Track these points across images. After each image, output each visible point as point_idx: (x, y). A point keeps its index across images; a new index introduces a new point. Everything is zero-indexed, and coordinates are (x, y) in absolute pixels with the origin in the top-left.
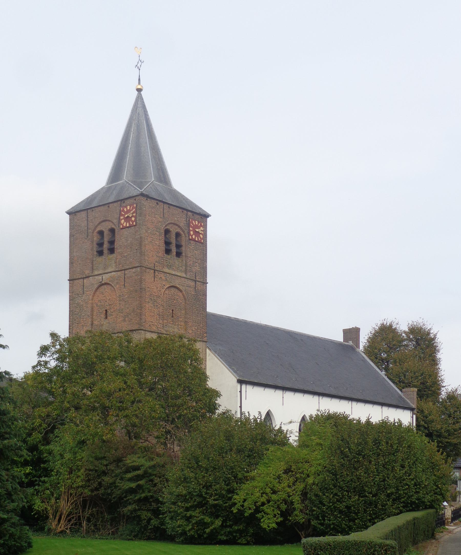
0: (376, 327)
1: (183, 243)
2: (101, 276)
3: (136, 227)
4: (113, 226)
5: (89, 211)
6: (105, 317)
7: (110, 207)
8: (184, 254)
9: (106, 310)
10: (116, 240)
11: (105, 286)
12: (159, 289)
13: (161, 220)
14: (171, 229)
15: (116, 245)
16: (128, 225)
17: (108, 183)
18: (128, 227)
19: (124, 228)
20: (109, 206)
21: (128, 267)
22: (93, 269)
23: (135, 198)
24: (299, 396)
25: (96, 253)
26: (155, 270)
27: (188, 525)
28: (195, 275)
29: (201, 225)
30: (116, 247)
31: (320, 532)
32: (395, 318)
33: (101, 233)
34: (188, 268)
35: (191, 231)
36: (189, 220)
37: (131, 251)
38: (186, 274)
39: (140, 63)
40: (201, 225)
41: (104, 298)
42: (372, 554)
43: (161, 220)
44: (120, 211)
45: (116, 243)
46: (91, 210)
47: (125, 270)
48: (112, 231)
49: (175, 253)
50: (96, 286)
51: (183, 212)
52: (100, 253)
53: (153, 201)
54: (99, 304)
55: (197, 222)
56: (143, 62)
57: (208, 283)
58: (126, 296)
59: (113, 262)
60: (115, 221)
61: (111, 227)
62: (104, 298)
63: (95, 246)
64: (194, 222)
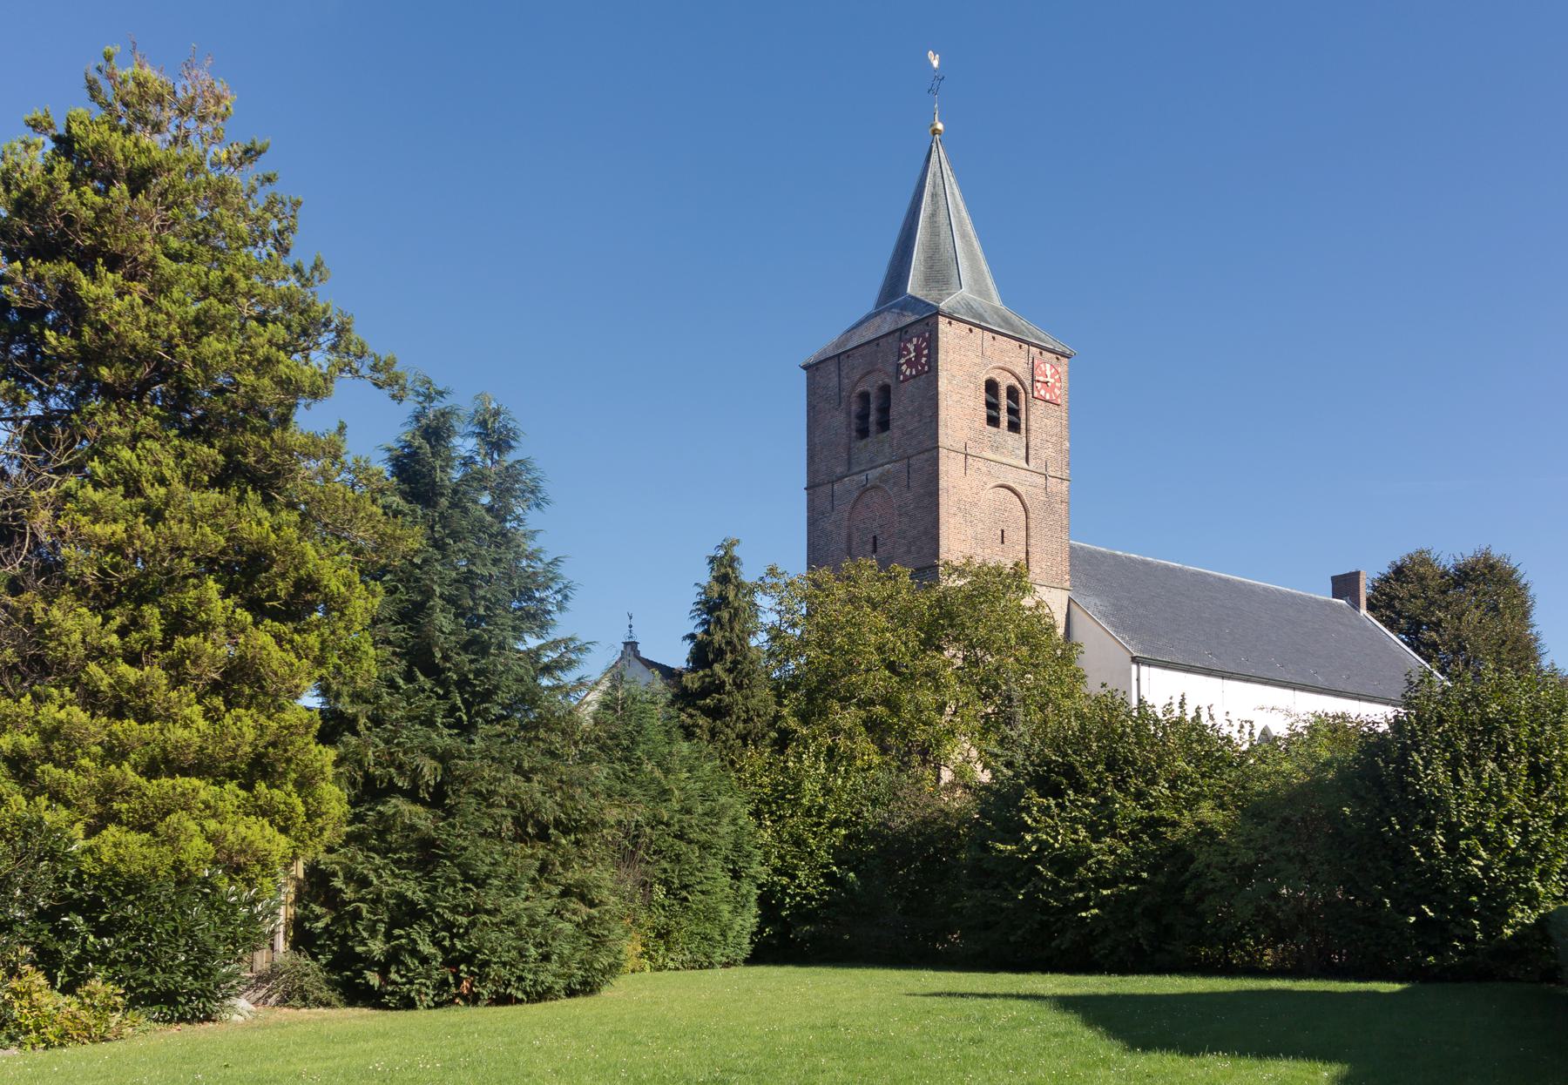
0: (1459, 558)
2: (865, 473)
3: (929, 374)
9: (875, 537)
12: (974, 490)
13: (978, 361)
16: (914, 373)
18: (914, 377)
19: (907, 379)
20: (878, 344)
22: (849, 463)
25: (854, 434)
27: (927, 674)
32: (1104, 685)
33: (865, 397)
39: (935, 87)
42: (5, 146)
43: (978, 361)
48: (885, 390)
51: (1020, 346)
52: (863, 433)
63: (854, 421)
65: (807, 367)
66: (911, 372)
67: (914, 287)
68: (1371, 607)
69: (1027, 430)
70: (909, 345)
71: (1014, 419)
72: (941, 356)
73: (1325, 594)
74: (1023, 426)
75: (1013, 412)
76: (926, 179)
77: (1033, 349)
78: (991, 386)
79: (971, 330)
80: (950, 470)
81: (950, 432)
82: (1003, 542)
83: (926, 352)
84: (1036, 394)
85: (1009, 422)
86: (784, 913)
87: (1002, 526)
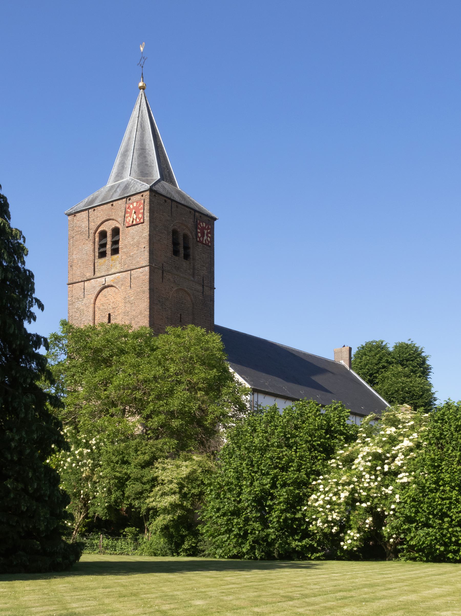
1: (191, 245)
2: (104, 278)
3: (143, 224)
4: (118, 225)
5: (90, 210)
6: (107, 321)
7: (114, 205)
8: (191, 257)
10: (120, 239)
11: (109, 289)
13: (169, 218)
14: (179, 230)
15: (121, 245)
20: (112, 205)
21: (134, 267)
23: (142, 194)
28: (203, 280)
29: (208, 227)
30: (120, 247)
31: (100, 534)
33: (103, 235)
34: (196, 272)
35: (199, 232)
36: (197, 221)
37: (138, 250)
38: (193, 277)
39: (143, 60)
40: (208, 227)
41: (107, 301)
43: (169, 218)
45: (120, 243)
46: (93, 209)
47: (131, 270)
49: (183, 255)
50: (98, 289)
51: (190, 212)
53: (161, 197)
54: (102, 307)
55: (204, 224)
56: (147, 58)
57: (215, 288)
58: (132, 298)
59: (118, 262)
60: (120, 219)
61: (115, 227)
62: (107, 301)
64: (201, 224)
79: (165, 201)
82: (181, 321)
86: (132, 510)
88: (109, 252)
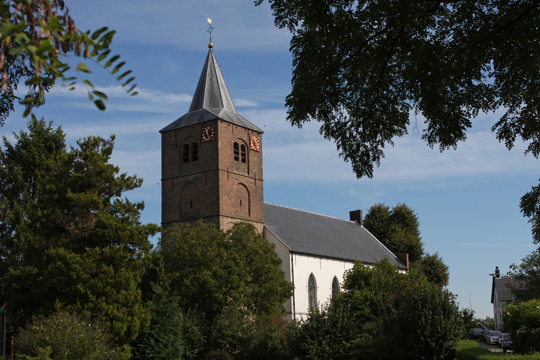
13: (231, 136)
17: (190, 111)
18: (208, 142)
20: (193, 127)
24: (331, 262)
25: (182, 160)
26: (228, 172)
33: (186, 146)
39: (211, 29)
43: (231, 136)
44: (202, 130)
48: (195, 145)
52: (186, 160)
65: (160, 132)
66: (207, 140)
67: (205, 106)
68: (364, 226)
69: (248, 162)
70: (206, 129)
71: (243, 158)
72: (219, 135)
73: (347, 218)
74: (247, 160)
75: (243, 155)
76: (207, 67)
77: (250, 131)
78: (236, 145)
79: (229, 125)
80: (222, 176)
81: (222, 163)
82: (241, 205)
83: (213, 133)
84: (251, 148)
85: (242, 159)
87: (240, 199)
88: (190, 159)
